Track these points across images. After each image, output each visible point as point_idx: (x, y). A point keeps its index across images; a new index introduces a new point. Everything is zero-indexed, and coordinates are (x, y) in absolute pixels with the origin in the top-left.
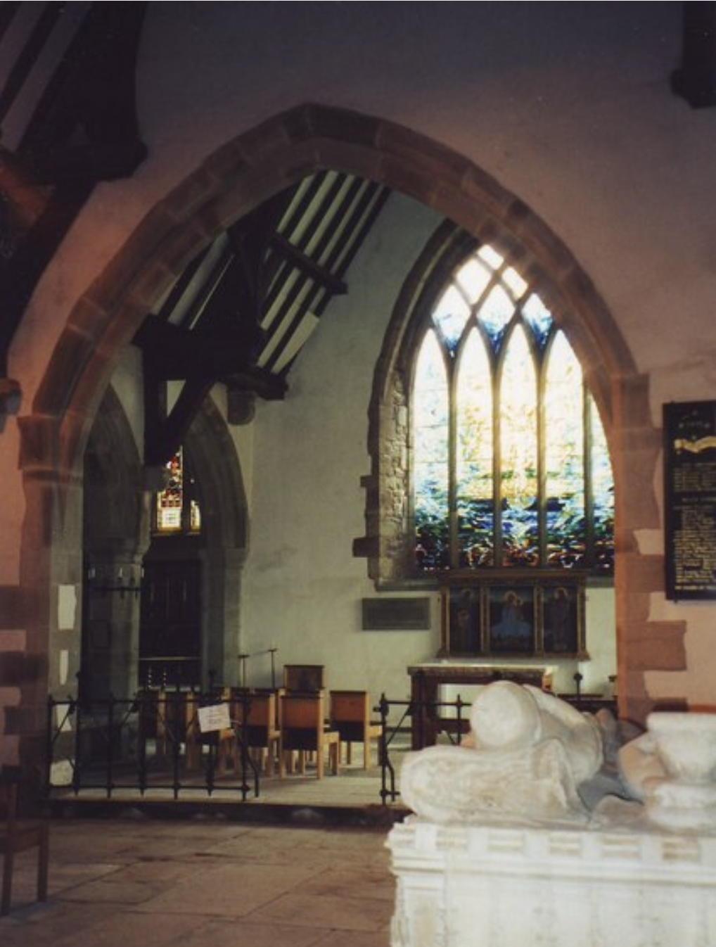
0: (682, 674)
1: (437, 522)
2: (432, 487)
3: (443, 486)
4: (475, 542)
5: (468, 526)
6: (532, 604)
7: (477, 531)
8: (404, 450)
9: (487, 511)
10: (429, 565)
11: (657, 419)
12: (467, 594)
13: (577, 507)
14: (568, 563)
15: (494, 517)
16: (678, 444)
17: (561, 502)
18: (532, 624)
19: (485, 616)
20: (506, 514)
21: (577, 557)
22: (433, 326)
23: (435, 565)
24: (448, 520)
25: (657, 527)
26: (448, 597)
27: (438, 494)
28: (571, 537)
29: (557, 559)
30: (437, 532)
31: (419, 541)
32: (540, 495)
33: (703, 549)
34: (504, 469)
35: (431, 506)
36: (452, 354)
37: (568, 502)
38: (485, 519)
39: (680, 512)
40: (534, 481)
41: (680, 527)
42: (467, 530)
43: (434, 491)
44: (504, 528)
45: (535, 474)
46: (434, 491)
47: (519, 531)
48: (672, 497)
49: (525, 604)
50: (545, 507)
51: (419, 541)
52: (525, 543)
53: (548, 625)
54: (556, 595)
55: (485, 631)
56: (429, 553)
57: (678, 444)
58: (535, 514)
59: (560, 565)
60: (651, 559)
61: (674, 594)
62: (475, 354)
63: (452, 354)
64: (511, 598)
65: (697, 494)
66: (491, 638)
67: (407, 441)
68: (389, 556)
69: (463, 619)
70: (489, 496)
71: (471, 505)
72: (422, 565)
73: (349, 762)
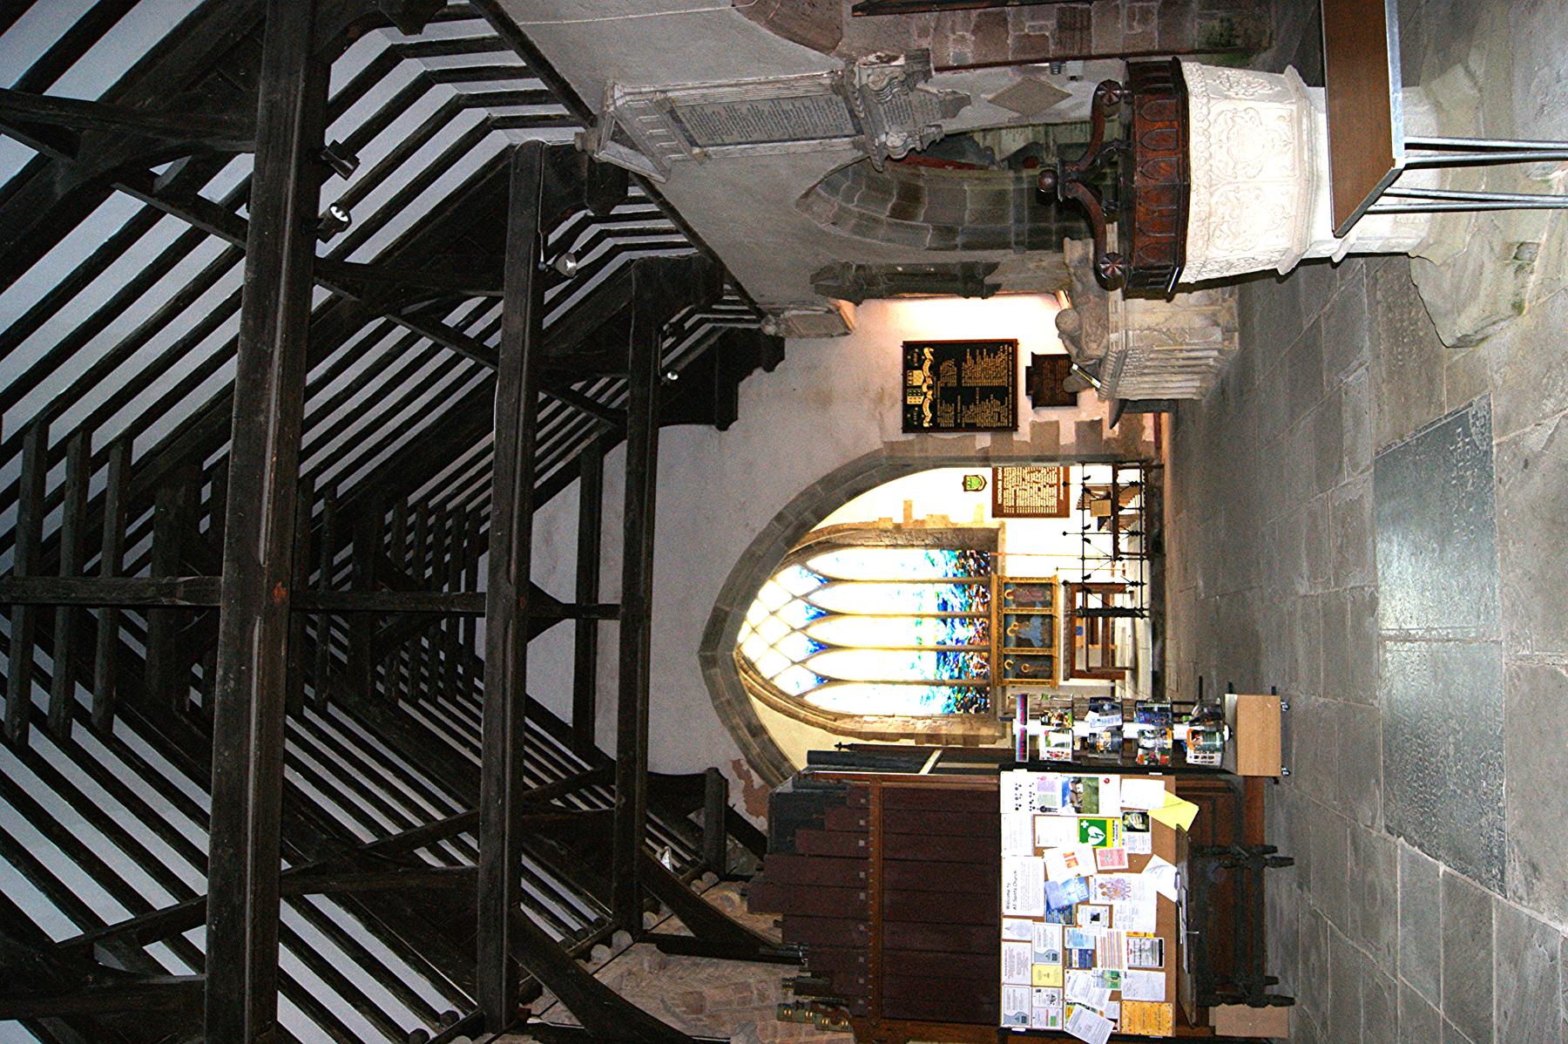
0: (1061, 423)
1: (952, 696)
2: (925, 699)
3: (926, 689)
4: (968, 666)
5: (956, 671)
6: (1017, 615)
7: (960, 665)
8: (895, 718)
9: (946, 656)
10: (986, 704)
11: (911, 436)
12: (1008, 664)
13: (947, 591)
14: (986, 597)
15: (950, 651)
16: (926, 425)
17: (941, 602)
18: (1032, 615)
19: (1026, 651)
20: (949, 642)
21: (982, 590)
22: (802, 696)
23: (986, 698)
24: (952, 686)
25: (974, 436)
26: (1011, 679)
27: (931, 695)
28: (967, 593)
29: (983, 604)
30: (960, 696)
31: (967, 711)
32: (936, 616)
33: (988, 411)
34: (915, 644)
35: (941, 700)
36: (825, 681)
37: (941, 597)
38: (951, 658)
39: (966, 424)
40: (925, 620)
41: (975, 424)
42: (960, 672)
43: (928, 698)
44: (960, 644)
45: (919, 619)
46: (928, 698)
47: (965, 632)
48: (957, 428)
49: (1017, 621)
50: (945, 614)
51: (967, 711)
52: (972, 628)
53: (1033, 604)
54: (1011, 598)
55: (1037, 651)
56: (976, 703)
57: (926, 425)
58: (949, 620)
59: (1022, 190)
60: (993, 441)
61: (1014, 427)
62: (826, 664)
63: (825, 681)
64: (1012, 631)
65: (956, 415)
66: (1042, 647)
67: (889, 717)
68: (979, 729)
69: (1027, 667)
70: (934, 654)
71: (940, 668)
72: (986, 709)
73: (1161, 941)
